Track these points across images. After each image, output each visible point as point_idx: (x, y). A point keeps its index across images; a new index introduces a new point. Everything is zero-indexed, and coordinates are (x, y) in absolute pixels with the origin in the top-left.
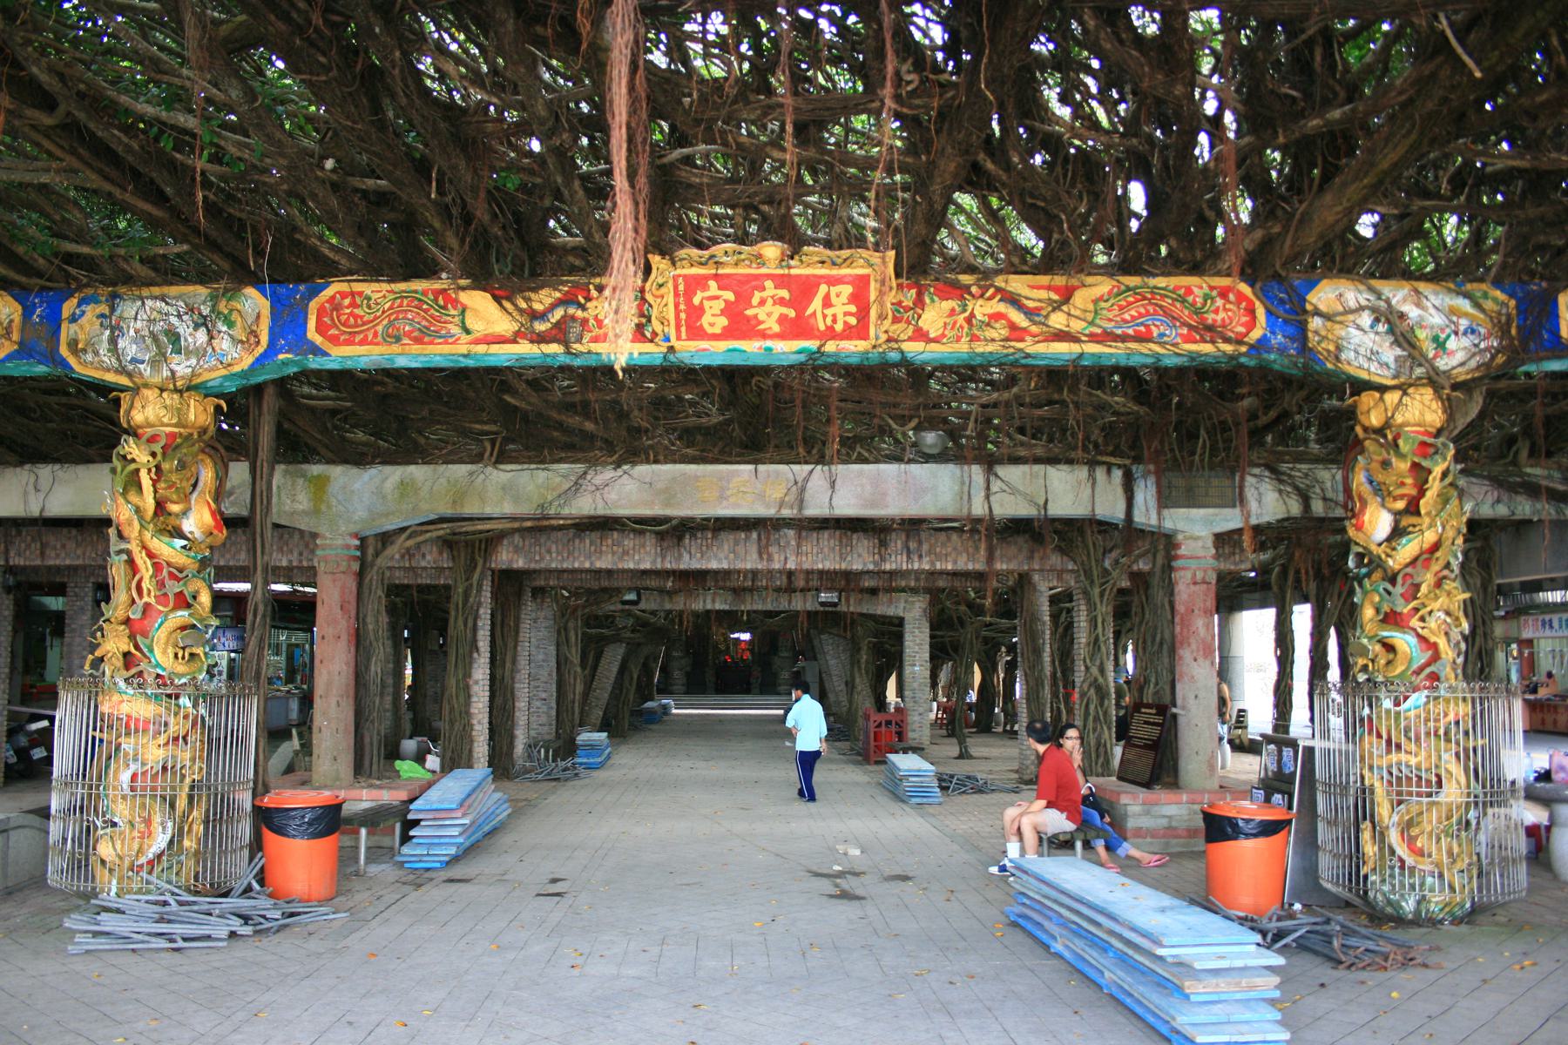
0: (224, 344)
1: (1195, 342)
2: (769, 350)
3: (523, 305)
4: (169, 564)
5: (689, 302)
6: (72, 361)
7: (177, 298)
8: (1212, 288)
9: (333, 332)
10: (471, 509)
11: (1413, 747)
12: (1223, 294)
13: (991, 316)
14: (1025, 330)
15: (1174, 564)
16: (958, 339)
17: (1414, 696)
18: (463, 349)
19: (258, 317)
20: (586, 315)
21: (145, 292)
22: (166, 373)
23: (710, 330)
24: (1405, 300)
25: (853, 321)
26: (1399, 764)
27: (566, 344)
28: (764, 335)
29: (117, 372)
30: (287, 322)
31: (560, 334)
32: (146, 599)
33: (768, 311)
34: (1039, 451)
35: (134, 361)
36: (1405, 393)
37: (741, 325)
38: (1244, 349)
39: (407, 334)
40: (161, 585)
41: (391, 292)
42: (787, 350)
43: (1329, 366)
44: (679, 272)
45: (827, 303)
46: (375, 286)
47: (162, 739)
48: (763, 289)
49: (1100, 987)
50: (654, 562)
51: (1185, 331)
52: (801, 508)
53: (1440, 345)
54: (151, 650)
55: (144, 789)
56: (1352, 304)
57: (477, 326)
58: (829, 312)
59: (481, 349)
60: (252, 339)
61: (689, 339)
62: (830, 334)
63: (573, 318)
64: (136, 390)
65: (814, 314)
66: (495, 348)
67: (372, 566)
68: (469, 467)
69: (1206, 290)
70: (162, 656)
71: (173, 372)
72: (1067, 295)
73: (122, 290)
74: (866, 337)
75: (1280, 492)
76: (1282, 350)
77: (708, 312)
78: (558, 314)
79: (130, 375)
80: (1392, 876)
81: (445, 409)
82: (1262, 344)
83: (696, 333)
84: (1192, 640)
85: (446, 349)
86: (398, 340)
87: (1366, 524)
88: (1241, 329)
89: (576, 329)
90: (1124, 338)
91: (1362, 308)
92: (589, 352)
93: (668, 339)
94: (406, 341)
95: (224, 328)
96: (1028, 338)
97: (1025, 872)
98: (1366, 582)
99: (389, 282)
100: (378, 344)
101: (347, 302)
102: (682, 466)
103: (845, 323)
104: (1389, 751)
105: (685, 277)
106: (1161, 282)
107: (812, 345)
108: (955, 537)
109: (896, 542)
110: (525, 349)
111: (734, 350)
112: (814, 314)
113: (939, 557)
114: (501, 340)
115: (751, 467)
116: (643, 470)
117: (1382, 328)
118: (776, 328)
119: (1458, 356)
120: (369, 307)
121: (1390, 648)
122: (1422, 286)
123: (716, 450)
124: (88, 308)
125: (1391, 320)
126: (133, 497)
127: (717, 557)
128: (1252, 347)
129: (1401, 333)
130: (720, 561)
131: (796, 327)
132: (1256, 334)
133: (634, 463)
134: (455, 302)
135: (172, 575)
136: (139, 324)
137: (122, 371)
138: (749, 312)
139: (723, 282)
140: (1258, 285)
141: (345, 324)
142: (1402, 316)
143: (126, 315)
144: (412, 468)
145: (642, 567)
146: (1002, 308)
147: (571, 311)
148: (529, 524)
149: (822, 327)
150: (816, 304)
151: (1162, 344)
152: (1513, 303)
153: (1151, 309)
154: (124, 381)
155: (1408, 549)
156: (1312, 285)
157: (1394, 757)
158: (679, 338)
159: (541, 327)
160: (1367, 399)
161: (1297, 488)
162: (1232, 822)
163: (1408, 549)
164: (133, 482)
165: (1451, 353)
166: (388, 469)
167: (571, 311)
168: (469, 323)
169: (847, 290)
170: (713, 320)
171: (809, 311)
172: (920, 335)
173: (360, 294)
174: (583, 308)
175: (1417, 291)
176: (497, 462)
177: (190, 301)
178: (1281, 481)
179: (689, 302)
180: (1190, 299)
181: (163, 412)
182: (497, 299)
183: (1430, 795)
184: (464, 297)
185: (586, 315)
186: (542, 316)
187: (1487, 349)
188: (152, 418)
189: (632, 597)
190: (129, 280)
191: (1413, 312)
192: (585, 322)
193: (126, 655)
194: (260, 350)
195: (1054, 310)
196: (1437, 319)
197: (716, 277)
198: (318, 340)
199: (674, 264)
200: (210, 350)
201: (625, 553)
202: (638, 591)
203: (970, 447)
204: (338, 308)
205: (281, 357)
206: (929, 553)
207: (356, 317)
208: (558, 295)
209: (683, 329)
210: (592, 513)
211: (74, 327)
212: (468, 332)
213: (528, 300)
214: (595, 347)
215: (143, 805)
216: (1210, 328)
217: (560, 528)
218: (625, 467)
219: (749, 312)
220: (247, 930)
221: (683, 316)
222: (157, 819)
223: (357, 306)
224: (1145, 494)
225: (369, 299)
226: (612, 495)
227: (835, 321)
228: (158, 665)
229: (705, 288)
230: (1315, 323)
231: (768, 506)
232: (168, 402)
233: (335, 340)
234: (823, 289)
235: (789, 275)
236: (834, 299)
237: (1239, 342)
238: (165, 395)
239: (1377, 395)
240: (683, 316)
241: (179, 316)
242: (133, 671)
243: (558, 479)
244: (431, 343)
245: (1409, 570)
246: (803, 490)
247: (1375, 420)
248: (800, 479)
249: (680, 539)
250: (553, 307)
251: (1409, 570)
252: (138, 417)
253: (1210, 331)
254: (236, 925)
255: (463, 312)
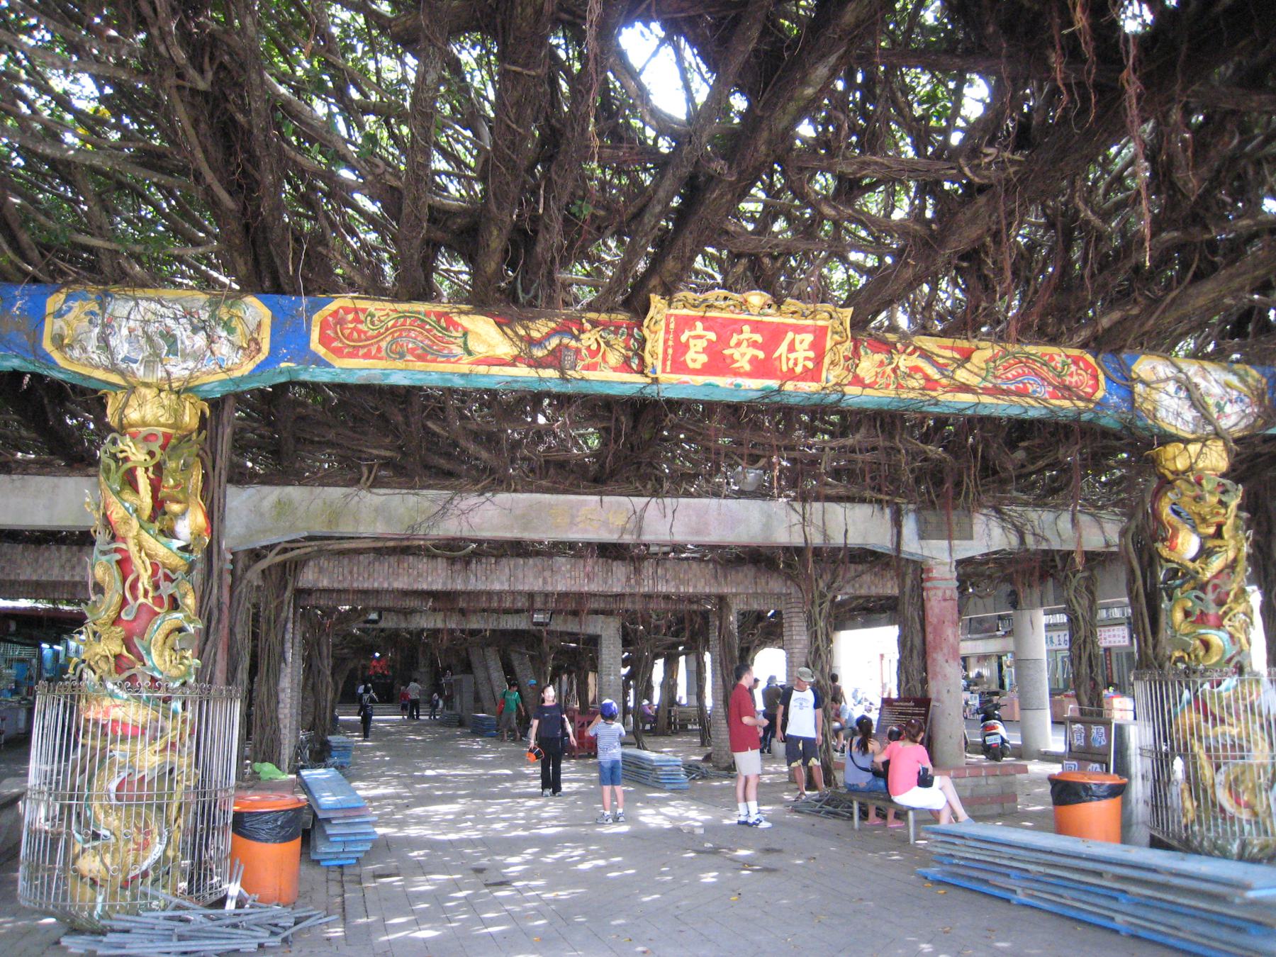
0: (223, 349)
1: (1058, 398)
2: (738, 386)
3: (522, 332)
4: (164, 565)
5: (677, 338)
6: (57, 356)
7: (175, 301)
8: (1068, 357)
9: (335, 344)
10: (346, 528)
11: (1234, 720)
12: (1075, 362)
13: (911, 369)
14: (936, 382)
15: (924, 585)
16: (888, 386)
17: (1228, 680)
18: (465, 369)
19: (259, 325)
20: (579, 345)
21: (139, 293)
22: (160, 373)
23: (691, 365)
24: (1196, 374)
25: (810, 365)
26: (1224, 734)
27: (562, 371)
28: (737, 373)
29: (106, 369)
30: (289, 335)
31: (555, 359)
32: (141, 600)
33: (742, 353)
34: (842, 491)
35: (126, 359)
36: (1204, 445)
37: (718, 363)
38: (1091, 406)
39: (412, 351)
40: (156, 587)
41: (395, 311)
42: (753, 386)
43: (1150, 422)
44: (672, 311)
45: (792, 349)
46: (378, 305)
47: (158, 746)
48: (741, 332)
49: (1116, 932)
50: (444, 584)
51: (1051, 389)
52: (639, 536)
53: (1220, 408)
54: (149, 653)
55: (130, 798)
56: (1162, 376)
57: (480, 349)
58: (792, 356)
59: (482, 369)
60: (253, 345)
61: (672, 372)
62: (791, 375)
63: (567, 347)
64: (132, 389)
65: (780, 356)
66: (495, 370)
67: (241, 579)
68: (344, 490)
69: (1063, 358)
70: (159, 660)
71: (168, 373)
72: (967, 356)
73: (114, 289)
74: (818, 380)
75: (1003, 528)
76: (1116, 407)
77: (692, 349)
78: (554, 342)
79: (122, 373)
80: (1216, 825)
81: (350, 434)
82: (1101, 404)
83: (679, 366)
84: (944, 645)
85: (448, 367)
86: (402, 356)
87: (1179, 546)
88: (1089, 390)
89: (569, 358)
90: (1007, 392)
91: (1168, 379)
92: (582, 379)
93: (654, 372)
94: (409, 357)
95: (224, 334)
96: (940, 389)
97: (962, 837)
98: (1178, 592)
99: (392, 301)
100: (380, 359)
101: (350, 317)
102: (538, 495)
103: (804, 366)
104: (1214, 725)
105: (676, 316)
106: (1031, 349)
107: (774, 384)
108: (694, 565)
109: (648, 568)
110: (523, 372)
111: (710, 385)
112: (780, 356)
113: (682, 582)
114: (501, 362)
115: (597, 498)
116: (503, 497)
117: (1183, 394)
118: (747, 367)
119: (1234, 417)
120: (372, 323)
121: (1207, 645)
122: (1207, 364)
123: (567, 483)
124: (76, 305)
125: (1189, 390)
126: (128, 495)
127: (498, 579)
128: (1097, 404)
129: (1196, 402)
130: (502, 583)
131: (761, 368)
132: (1099, 394)
133: (495, 492)
134: (456, 325)
135: (167, 577)
136: (132, 324)
137: (113, 368)
138: (727, 352)
139: (709, 324)
140: (1100, 357)
141: (349, 338)
142: (1196, 385)
143: (117, 314)
144: (289, 489)
145: (434, 588)
146: (922, 363)
147: (566, 341)
148: (391, 544)
149: (785, 369)
150: (783, 349)
151: (1036, 399)
152: (1264, 381)
153: (1026, 370)
154: (115, 379)
155: (1217, 563)
156: (1135, 359)
157: (1219, 729)
158: (664, 371)
159: (539, 353)
160: (1172, 449)
161: (1014, 525)
162: (1086, 787)
163: (1217, 563)
164: (130, 481)
165: (1227, 416)
166: (266, 489)
167: (566, 341)
168: (471, 345)
169: (809, 338)
170: (696, 357)
171: (776, 355)
172: (857, 381)
173: (364, 310)
174: (578, 339)
175: (1204, 369)
176: (373, 486)
177: (188, 305)
178: (1003, 520)
179: (677, 338)
180: (1053, 364)
181: (161, 412)
182: (499, 325)
183: (1242, 758)
184: (465, 321)
185: (579, 345)
186: (539, 343)
187: (1250, 414)
188: (149, 417)
189: (374, 616)
190: (122, 278)
191: (1203, 384)
192: (578, 351)
193: (118, 657)
194: (261, 357)
195: (958, 367)
196: (1217, 390)
197: (703, 319)
198: (322, 351)
199: (670, 305)
200: (209, 353)
201: (419, 575)
202: (380, 611)
203: (801, 482)
204: (341, 322)
205: (283, 365)
206: (674, 578)
207: (360, 332)
208: (553, 325)
209: (669, 363)
210: (458, 535)
211: (59, 323)
212: (469, 353)
213: (526, 328)
214: (590, 375)
215: (138, 815)
216: (1068, 388)
217: (358, 552)
218: (488, 495)
219: (727, 352)
220: (276, 941)
221: (670, 351)
222: (154, 826)
223: (361, 322)
224: (909, 526)
225: (373, 316)
226: (476, 519)
227: (795, 364)
228: (154, 668)
229: (692, 327)
230: (1139, 388)
231: (611, 532)
232: (166, 402)
233: (338, 352)
234: (790, 335)
235: (761, 322)
236: (797, 346)
237: (1089, 401)
238: (163, 395)
239: (1182, 446)
240: (670, 351)
241: (176, 319)
242: (126, 674)
243: (427, 504)
244: (434, 361)
245: (1216, 581)
246: (641, 518)
247: (1181, 464)
248: (638, 510)
249: (468, 563)
250: (548, 336)
251: (1216, 581)
252: (133, 415)
253: (1067, 390)
254: (263, 935)
255: (465, 334)
